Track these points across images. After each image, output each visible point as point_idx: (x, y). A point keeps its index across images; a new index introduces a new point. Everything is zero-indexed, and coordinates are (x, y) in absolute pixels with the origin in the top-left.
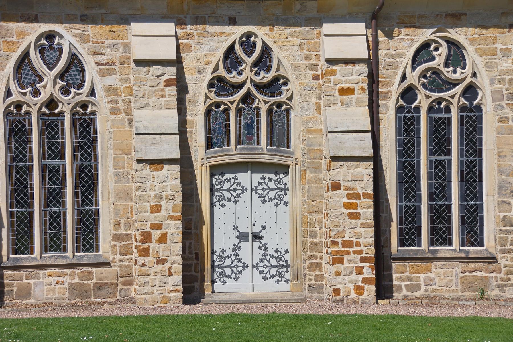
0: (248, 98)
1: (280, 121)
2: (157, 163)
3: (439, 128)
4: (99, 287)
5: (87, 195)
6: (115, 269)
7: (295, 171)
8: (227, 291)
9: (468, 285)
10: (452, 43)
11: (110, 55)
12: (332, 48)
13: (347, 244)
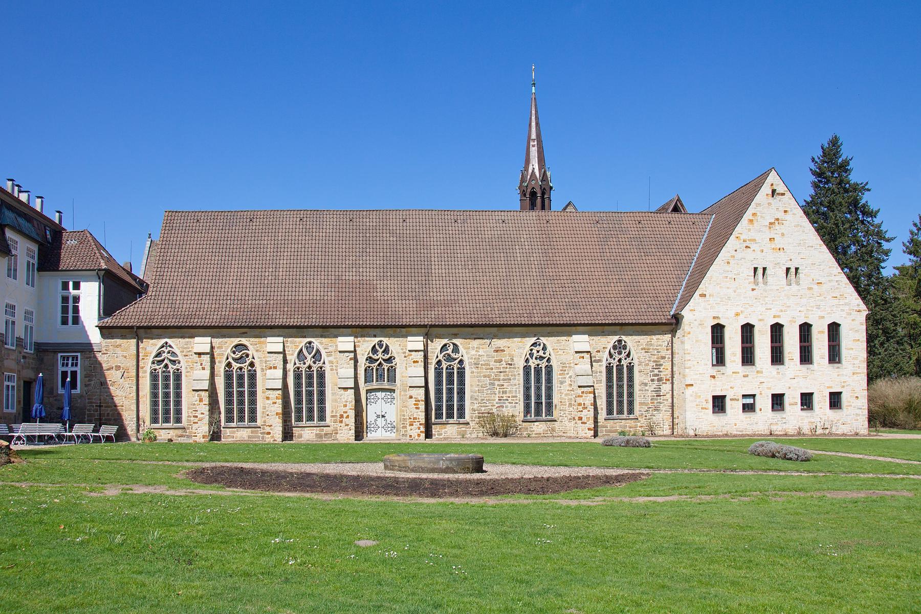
0: (380, 364)
1: (392, 371)
2: (346, 389)
3: (450, 375)
4: (326, 434)
5: (322, 401)
6: (331, 428)
7: (397, 391)
8: (371, 436)
9: (459, 433)
10: (454, 344)
11: (331, 349)
12: (411, 346)
13: (415, 418)
